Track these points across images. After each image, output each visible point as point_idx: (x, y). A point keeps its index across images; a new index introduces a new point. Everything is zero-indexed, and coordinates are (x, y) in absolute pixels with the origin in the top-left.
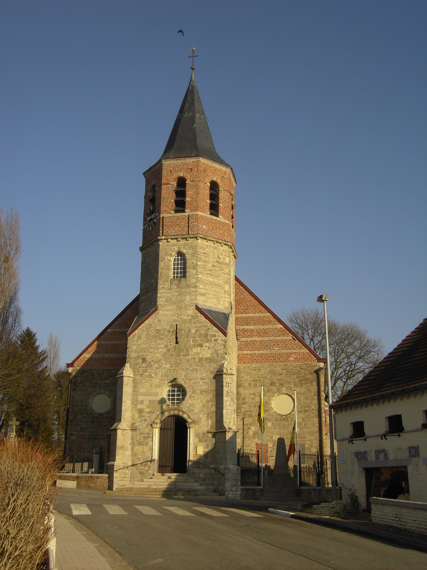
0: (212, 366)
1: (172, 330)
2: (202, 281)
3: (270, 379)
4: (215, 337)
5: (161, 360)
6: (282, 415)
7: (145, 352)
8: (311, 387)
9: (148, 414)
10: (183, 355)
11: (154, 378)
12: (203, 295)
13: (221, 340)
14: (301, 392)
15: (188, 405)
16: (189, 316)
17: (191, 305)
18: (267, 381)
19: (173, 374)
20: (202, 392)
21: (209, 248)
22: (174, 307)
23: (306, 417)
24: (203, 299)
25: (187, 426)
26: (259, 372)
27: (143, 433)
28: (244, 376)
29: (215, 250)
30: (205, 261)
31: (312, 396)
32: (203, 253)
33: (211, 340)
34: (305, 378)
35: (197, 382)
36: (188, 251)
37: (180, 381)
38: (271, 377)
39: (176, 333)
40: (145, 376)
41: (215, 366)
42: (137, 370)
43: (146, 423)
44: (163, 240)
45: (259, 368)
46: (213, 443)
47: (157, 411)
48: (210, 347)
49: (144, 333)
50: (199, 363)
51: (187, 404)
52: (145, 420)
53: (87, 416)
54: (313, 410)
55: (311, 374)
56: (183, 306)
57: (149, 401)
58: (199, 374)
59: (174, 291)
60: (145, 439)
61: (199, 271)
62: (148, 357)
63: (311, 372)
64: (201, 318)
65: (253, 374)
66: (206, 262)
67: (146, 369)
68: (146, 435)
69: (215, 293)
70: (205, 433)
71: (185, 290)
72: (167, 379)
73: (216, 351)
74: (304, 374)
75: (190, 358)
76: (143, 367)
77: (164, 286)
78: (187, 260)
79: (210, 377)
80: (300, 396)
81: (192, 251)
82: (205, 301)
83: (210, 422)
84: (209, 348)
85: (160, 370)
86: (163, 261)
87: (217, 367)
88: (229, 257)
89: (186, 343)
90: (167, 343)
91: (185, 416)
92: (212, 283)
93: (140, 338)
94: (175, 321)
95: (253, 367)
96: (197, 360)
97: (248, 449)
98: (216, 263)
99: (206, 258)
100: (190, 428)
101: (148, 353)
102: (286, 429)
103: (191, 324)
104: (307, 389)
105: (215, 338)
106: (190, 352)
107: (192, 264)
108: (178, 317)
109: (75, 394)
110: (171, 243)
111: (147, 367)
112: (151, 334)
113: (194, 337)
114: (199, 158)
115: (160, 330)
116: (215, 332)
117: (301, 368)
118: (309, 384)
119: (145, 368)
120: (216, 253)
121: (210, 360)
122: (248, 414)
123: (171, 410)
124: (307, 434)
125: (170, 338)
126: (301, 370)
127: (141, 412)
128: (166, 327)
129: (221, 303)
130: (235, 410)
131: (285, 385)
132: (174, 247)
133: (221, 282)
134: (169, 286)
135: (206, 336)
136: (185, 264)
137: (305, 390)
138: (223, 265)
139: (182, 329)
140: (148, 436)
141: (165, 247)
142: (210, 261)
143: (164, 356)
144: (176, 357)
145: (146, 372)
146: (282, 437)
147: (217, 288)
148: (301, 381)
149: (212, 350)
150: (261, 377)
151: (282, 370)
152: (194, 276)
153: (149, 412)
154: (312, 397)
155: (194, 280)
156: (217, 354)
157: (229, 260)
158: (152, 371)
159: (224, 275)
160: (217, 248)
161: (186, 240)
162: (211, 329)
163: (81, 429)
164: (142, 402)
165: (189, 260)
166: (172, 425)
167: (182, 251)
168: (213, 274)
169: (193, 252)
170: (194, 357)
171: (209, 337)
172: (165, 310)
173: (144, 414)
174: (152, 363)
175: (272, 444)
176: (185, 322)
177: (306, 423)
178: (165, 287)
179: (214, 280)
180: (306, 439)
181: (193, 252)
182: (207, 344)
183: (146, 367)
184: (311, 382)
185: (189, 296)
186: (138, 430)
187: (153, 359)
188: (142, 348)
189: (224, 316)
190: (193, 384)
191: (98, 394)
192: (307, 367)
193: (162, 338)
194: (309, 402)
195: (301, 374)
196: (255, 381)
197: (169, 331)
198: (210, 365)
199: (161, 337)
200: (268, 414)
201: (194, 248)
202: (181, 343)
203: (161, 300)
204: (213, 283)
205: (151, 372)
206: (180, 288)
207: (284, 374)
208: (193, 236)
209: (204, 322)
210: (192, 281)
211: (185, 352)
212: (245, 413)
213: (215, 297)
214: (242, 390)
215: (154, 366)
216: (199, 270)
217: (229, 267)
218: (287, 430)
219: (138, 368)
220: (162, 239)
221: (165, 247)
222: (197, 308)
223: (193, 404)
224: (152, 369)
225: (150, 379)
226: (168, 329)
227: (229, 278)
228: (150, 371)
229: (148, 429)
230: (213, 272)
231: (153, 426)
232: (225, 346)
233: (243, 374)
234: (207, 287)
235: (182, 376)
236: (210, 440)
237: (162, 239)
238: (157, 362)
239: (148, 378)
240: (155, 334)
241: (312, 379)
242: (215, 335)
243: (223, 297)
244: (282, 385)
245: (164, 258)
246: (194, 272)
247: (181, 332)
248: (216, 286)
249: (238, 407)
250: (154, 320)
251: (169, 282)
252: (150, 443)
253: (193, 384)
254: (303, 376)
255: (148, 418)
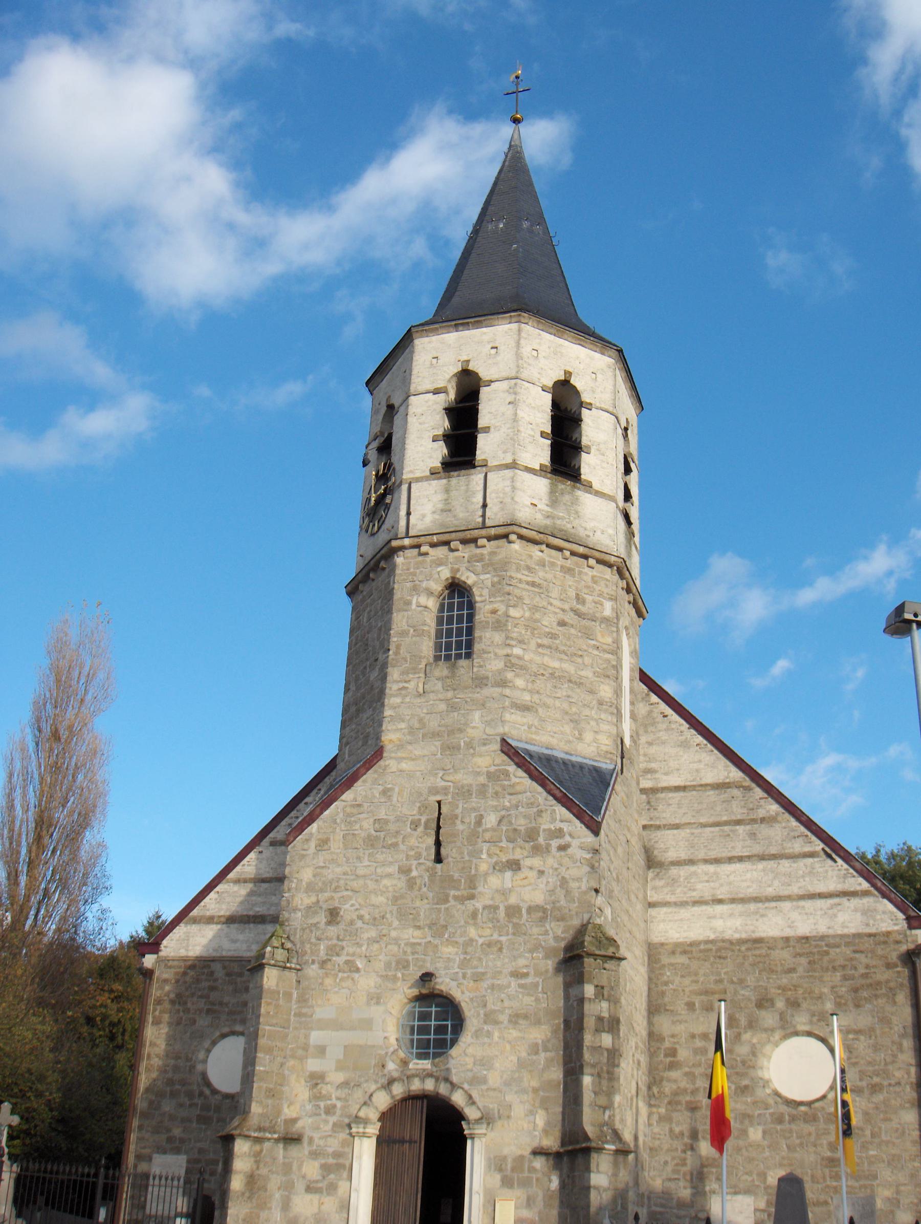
0: (550, 932)
1: (423, 819)
2: (522, 668)
3: (755, 987)
4: (561, 838)
5: (388, 916)
6: (795, 1101)
7: (336, 890)
8: (889, 1008)
9: (339, 1091)
10: (456, 898)
11: (362, 972)
12: (525, 708)
13: (581, 848)
14: (856, 1024)
15: (469, 1061)
16: (478, 774)
17: (487, 739)
18: (747, 994)
19: (424, 961)
20: (516, 1018)
21: (547, 568)
22: (435, 746)
23: (877, 1108)
24: (525, 720)
25: (464, 1130)
26: (720, 966)
27: (320, 1153)
28: (671, 978)
29: (567, 576)
30: (535, 609)
31: (896, 1038)
32: (528, 583)
33: (547, 849)
34: (869, 981)
35: (499, 985)
36: (482, 577)
37: (445, 984)
38: (758, 981)
39: (439, 827)
40: (334, 966)
41: (559, 932)
42: (311, 948)
43: (332, 1119)
44: (406, 551)
45: (718, 954)
46: (549, 1189)
47: (367, 1081)
48: (544, 869)
49: (338, 830)
50: (509, 922)
51: (467, 1059)
52: (329, 1111)
53: (188, 1103)
54: (899, 1084)
55: (889, 966)
56: (462, 744)
57: (345, 1047)
58: (506, 960)
59: (435, 698)
60: (325, 1173)
61: (514, 635)
62: (347, 906)
63: (890, 960)
64: (517, 780)
65: (702, 972)
66: (537, 611)
67: (340, 943)
68: (331, 1161)
69: (565, 706)
70: (522, 1157)
71: (470, 695)
72: (403, 975)
73: (564, 882)
74: (867, 967)
75: (479, 905)
76: (331, 939)
77: (406, 685)
78: (477, 605)
79: (543, 969)
80: (853, 1039)
81: (494, 576)
82: (533, 729)
83: (540, 1119)
84: (541, 873)
85: (383, 946)
86: (406, 611)
87: (566, 935)
88: (614, 599)
89: (467, 858)
90: (407, 859)
91: (458, 1099)
92: (556, 675)
93: (326, 847)
94: (434, 790)
95: (701, 951)
96: (502, 913)
97: (685, 1216)
98: (572, 614)
99: (537, 599)
100: (473, 1138)
101: (349, 893)
102: (812, 1149)
103: (485, 797)
104: (878, 1017)
105: (562, 842)
106: (480, 889)
107: (493, 615)
108: (444, 777)
109: (159, 1034)
110: (431, 558)
111: (341, 937)
112: (360, 831)
113: (495, 839)
114: (520, 315)
115: (386, 822)
116: (562, 821)
117: (854, 948)
118: (884, 1000)
119: (335, 941)
120: (570, 586)
121: (544, 911)
122: (684, 1102)
123: (414, 1076)
124: (882, 1165)
125: (417, 844)
126: (857, 955)
127: (317, 1084)
128: (405, 811)
129: (588, 736)
130: (644, 1088)
131: (804, 1005)
132: (439, 569)
133: (587, 673)
134: (421, 685)
135: (531, 835)
136: (471, 617)
137: (870, 1019)
138: (593, 623)
139: (456, 817)
140: (337, 1164)
141: (412, 570)
142: (549, 607)
143: (396, 901)
144: (433, 904)
145: (338, 955)
146: (798, 1172)
147: (572, 690)
148: (856, 990)
149: (550, 880)
150: (725, 981)
151: (795, 957)
152: (497, 651)
153: (342, 1083)
154: (893, 1042)
155: (497, 662)
156: (568, 893)
157: (613, 609)
158: (358, 950)
159: (596, 652)
160: (573, 570)
161: (477, 547)
162: (549, 812)
163: (170, 1140)
164: (321, 1051)
165: (483, 604)
166: (415, 1130)
167: (463, 578)
168: (562, 648)
169: (496, 579)
170: (491, 903)
171: (541, 840)
172: (404, 758)
173: (325, 1089)
174: (359, 924)
175: (766, 1197)
176: (464, 792)
177: (876, 1129)
178: (407, 688)
179: (566, 666)
180: (878, 1181)
181: (496, 579)
182: (536, 862)
183: (338, 939)
184: (890, 995)
185: (480, 712)
186: (305, 1140)
187: (362, 912)
188: (330, 877)
189: (595, 775)
190: (486, 990)
191: (224, 1036)
192: (876, 945)
193: (391, 845)
194: (885, 1060)
195: (855, 968)
196: (706, 992)
197: (415, 825)
198: (543, 929)
199: (390, 842)
200: (749, 1100)
201: (500, 568)
202: (450, 859)
203: (394, 727)
204: (561, 674)
205: (353, 955)
206: (455, 690)
207: (800, 970)
208: (497, 533)
209: (525, 792)
210: (490, 667)
211: (465, 889)
212: (677, 1098)
213: (567, 718)
214: (664, 1025)
215: (365, 936)
216: (514, 632)
217: (615, 629)
218: (815, 1152)
219: (313, 940)
220: (402, 548)
221: (412, 570)
222: (509, 750)
223: (484, 1057)
224: (357, 943)
225: (348, 977)
226: (411, 818)
227: (615, 663)
228: (351, 950)
229: (336, 1141)
230: (561, 642)
231: (354, 1130)
232: (593, 867)
233: (668, 974)
234: (540, 684)
235: (453, 967)
236: (537, 1179)
237: (402, 548)
238: (374, 921)
239: (344, 972)
240: (373, 832)
241: (892, 984)
242: (560, 830)
243: (592, 719)
244: (794, 1004)
245: (409, 603)
246: (498, 638)
247: (454, 823)
248: (571, 685)
249: (654, 1078)
250: (371, 789)
251: (419, 673)
252: (343, 1186)
253: (486, 990)
254: (865, 976)
255: (339, 1104)
